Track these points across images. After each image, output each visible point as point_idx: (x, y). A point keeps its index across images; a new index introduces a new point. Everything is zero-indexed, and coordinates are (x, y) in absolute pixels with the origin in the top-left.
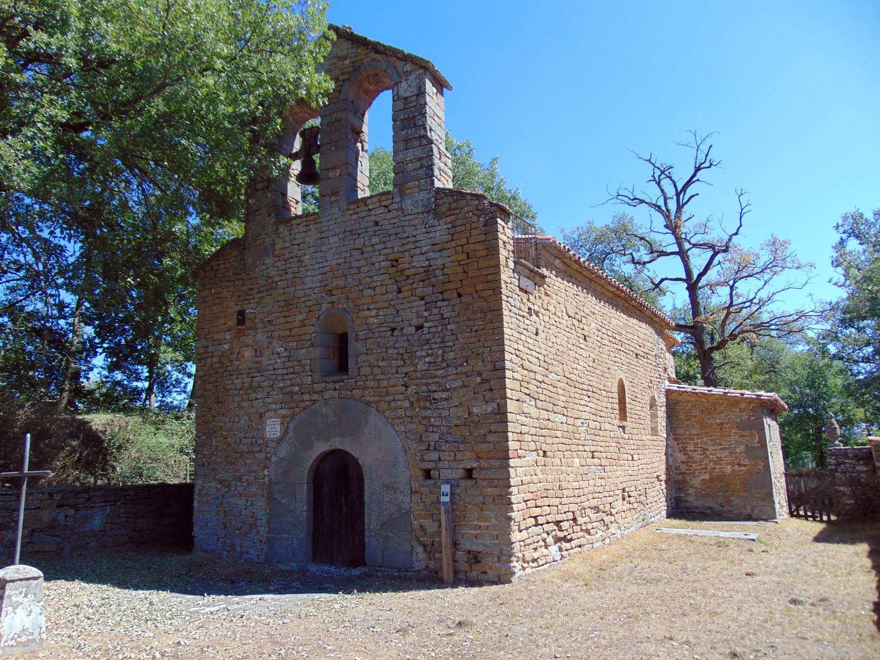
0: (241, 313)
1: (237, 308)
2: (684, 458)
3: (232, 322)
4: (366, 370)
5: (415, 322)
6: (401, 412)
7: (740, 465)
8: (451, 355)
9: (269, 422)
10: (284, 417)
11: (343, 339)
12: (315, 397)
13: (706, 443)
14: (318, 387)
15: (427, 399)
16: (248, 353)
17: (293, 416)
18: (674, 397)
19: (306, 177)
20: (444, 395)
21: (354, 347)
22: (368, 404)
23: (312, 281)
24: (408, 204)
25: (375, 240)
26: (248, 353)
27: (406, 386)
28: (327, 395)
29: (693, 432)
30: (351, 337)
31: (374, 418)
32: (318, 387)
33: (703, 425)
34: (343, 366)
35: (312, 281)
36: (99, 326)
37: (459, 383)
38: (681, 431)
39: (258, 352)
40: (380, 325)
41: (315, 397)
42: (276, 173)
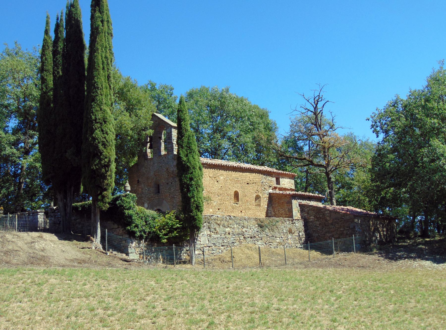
0: (138, 180)
1: (137, 179)
2: (274, 214)
3: (136, 182)
4: (163, 192)
5: (171, 182)
6: (169, 200)
7: (287, 214)
8: (177, 189)
9: (145, 204)
10: (148, 203)
11: (159, 185)
12: (154, 198)
13: (279, 209)
14: (154, 196)
15: (173, 197)
16: (140, 190)
17: (150, 202)
18: (272, 195)
19: (150, 148)
20: (176, 196)
21: (161, 187)
22: (163, 199)
23: (152, 174)
24: (169, 157)
25: (163, 164)
26: (140, 190)
27: (170, 195)
28: (156, 198)
29: (276, 205)
30: (160, 185)
31: (164, 202)
32: (154, 196)
33: (278, 203)
34: (159, 192)
35: (152, 174)
36: (186, 217)
37: (178, 194)
38: (273, 205)
39: (142, 189)
40: (165, 183)
41: (154, 198)
42: (144, 151)
